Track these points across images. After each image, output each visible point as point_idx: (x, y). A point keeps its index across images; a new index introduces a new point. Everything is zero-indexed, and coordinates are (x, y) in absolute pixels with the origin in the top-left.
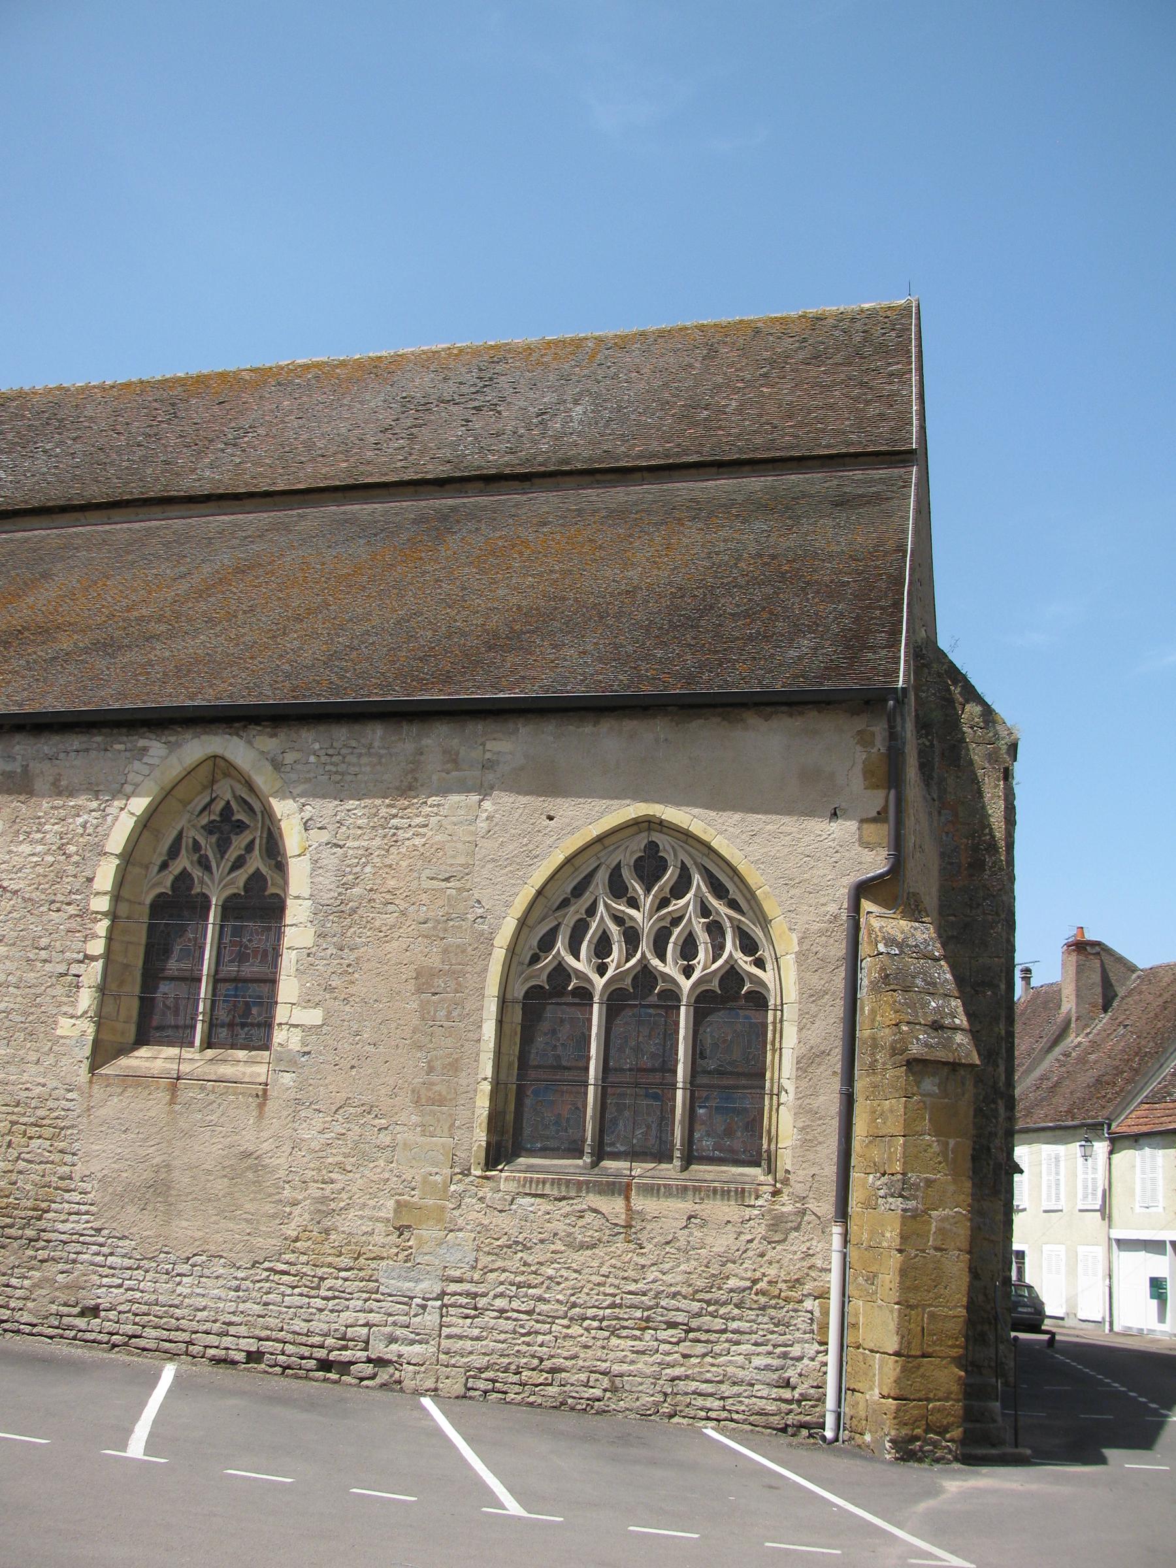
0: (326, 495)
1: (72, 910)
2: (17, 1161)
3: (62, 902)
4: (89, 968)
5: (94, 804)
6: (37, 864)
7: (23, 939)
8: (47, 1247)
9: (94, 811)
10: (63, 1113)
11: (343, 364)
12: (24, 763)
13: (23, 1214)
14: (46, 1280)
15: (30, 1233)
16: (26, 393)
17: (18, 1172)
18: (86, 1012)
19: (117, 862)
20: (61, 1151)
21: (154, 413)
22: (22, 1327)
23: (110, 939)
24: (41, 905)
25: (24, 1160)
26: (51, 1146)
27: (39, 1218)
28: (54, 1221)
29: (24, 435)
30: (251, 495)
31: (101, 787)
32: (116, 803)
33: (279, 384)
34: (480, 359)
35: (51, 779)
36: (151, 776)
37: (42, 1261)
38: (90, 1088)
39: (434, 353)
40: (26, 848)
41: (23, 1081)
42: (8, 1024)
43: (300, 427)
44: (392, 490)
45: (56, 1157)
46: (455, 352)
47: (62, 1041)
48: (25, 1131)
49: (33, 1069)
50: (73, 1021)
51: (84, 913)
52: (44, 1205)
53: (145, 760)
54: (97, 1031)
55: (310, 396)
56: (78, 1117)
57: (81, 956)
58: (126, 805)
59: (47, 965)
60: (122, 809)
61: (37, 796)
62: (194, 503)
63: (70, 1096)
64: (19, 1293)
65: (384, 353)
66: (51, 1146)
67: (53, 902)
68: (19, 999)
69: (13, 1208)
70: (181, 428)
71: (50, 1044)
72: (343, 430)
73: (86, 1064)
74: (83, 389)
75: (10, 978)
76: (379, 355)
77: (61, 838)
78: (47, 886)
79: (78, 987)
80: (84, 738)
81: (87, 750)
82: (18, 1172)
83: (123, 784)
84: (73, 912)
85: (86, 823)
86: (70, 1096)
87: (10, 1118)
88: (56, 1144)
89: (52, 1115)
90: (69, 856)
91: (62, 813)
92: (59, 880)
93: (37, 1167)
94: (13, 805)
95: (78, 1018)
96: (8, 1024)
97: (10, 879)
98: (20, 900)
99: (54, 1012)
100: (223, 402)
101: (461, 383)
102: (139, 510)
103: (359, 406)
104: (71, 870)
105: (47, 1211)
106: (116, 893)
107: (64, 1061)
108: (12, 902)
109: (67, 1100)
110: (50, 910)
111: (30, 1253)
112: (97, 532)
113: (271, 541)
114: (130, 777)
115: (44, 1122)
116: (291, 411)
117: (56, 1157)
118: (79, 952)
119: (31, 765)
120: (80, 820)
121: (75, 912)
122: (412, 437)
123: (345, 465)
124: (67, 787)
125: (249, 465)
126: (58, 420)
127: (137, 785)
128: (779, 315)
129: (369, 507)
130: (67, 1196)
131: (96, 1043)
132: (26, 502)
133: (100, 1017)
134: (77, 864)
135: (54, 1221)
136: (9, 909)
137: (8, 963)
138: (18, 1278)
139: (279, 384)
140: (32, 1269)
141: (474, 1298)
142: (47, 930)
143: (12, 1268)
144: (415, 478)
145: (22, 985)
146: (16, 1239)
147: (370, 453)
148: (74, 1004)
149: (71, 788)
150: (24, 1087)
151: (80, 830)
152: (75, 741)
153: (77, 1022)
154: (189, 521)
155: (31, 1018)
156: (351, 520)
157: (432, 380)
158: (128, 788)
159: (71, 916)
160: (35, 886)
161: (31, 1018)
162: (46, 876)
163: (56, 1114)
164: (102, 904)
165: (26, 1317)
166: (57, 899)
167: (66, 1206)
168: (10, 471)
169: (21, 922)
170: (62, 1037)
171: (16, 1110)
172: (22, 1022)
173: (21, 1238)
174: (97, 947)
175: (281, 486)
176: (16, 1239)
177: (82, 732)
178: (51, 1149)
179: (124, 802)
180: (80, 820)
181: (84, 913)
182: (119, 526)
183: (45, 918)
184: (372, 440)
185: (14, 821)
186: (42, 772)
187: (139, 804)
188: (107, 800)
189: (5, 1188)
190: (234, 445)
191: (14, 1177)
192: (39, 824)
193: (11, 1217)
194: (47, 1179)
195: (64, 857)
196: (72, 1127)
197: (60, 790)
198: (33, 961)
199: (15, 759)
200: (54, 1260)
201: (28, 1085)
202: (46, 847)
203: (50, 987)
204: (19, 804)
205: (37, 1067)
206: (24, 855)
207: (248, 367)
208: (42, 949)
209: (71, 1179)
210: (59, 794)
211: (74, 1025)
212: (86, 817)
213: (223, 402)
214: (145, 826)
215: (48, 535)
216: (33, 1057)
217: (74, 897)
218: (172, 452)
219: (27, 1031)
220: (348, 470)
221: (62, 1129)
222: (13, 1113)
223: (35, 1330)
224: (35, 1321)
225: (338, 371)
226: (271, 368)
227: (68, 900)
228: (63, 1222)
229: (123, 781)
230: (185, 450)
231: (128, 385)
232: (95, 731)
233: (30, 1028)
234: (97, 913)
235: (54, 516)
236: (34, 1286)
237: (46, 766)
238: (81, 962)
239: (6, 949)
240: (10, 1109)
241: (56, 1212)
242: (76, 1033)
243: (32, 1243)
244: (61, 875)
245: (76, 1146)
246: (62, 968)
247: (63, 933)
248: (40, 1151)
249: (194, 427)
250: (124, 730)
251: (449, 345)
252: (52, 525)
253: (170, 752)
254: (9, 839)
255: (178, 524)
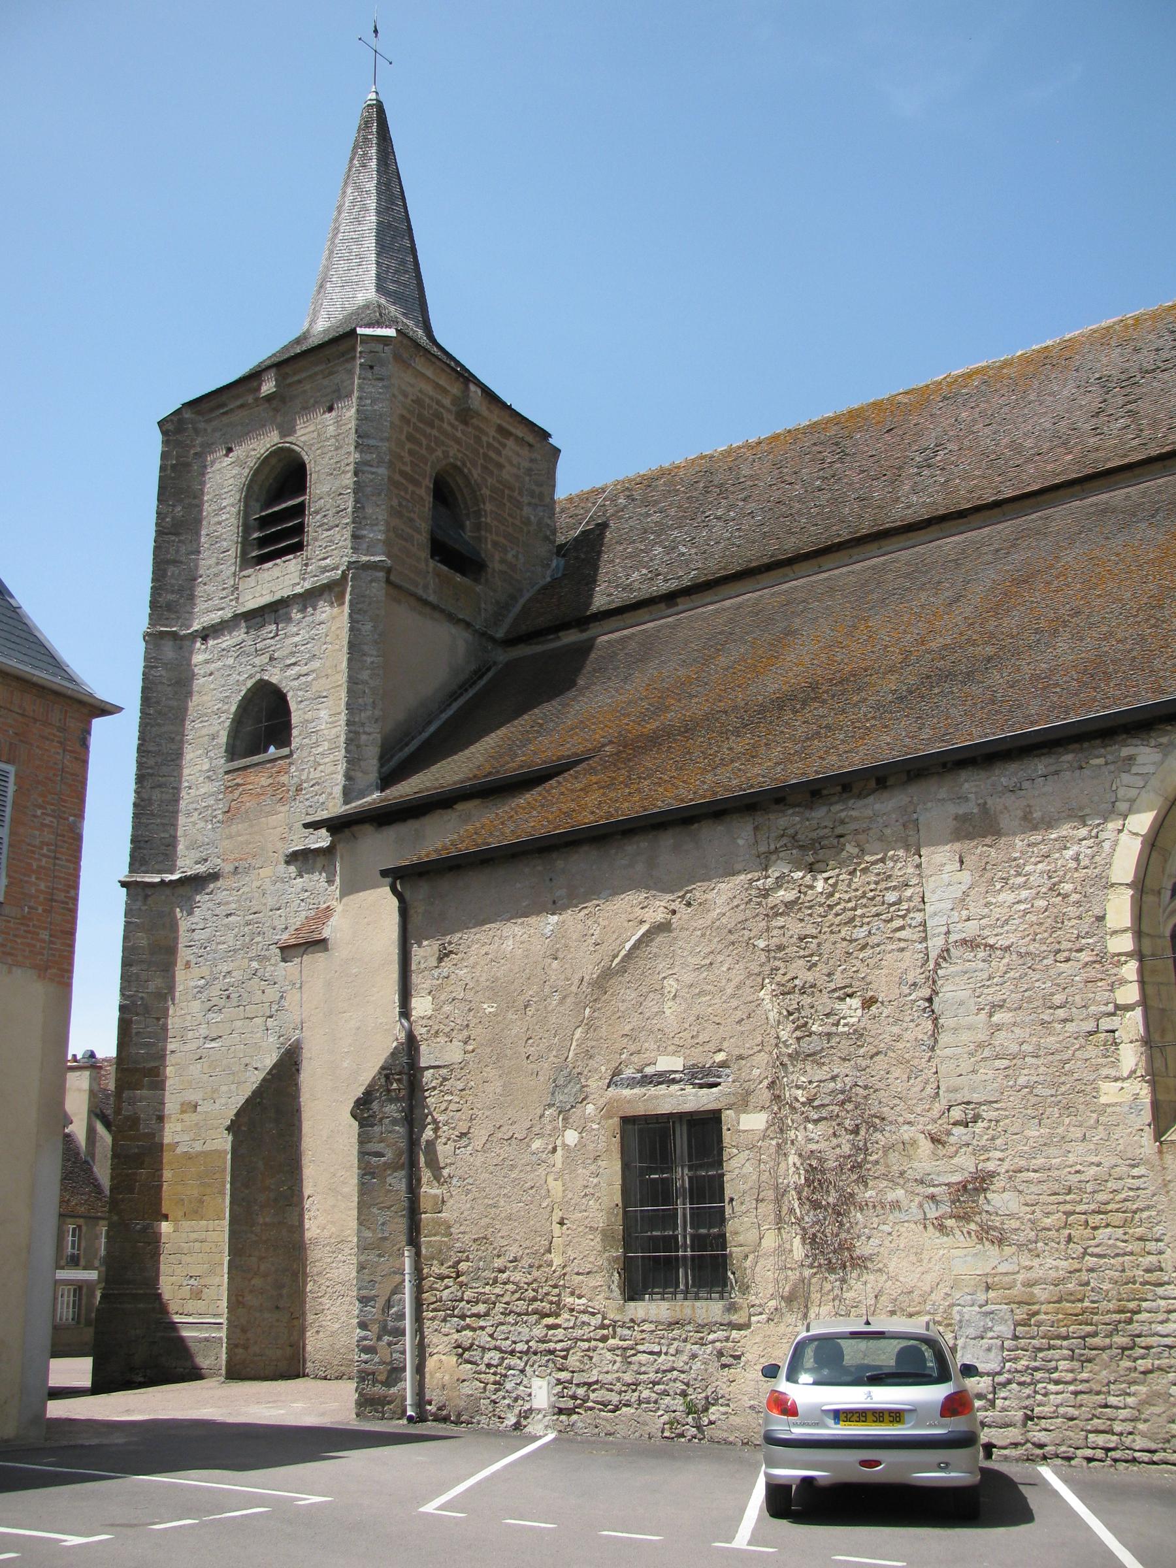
0: (1061, 493)
1: (1085, 956)
2: (1083, 1258)
3: (1070, 950)
4: (1125, 1020)
5: (1083, 832)
6: (1026, 913)
7: (1030, 1000)
8: (1148, 1354)
9: (1085, 839)
10: (1131, 1193)
11: (1007, 364)
12: (980, 801)
13: (1107, 1318)
14: (1158, 1395)
15: (1120, 1340)
16: (669, 470)
17: (1088, 1270)
18: (1134, 1072)
19: (1130, 892)
20: (1140, 1239)
21: (820, 456)
22: (1137, 1454)
23: (1142, 982)
24: (1044, 958)
25: (1092, 1255)
26: (1125, 1234)
27: (1130, 1321)
28: (1150, 1323)
29: (688, 508)
30: (977, 509)
31: (1087, 811)
32: (1111, 826)
33: (945, 398)
34: (1165, 322)
35: (1020, 813)
36: (1148, 787)
37: (1144, 1373)
38: (1161, 1159)
39: (1108, 328)
40: (1007, 897)
41: (1071, 1163)
42: (1033, 1100)
43: (994, 433)
44: (1137, 471)
45: (1135, 1246)
46: (1130, 322)
47: (1109, 1110)
48: (1087, 1222)
49: (1080, 1148)
50: (1119, 1084)
51: (1102, 957)
52: (1132, 1305)
53: (1134, 770)
54: (1154, 1092)
55: (987, 402)
56: (1154, 1195)
57: (1111, 1007)
58: (1124, 825)
59: (1068, 1025)
60: (1120, 831)
61: (1007, 835)
62: (913, 531)
63: (1135, 1172)
64: (1123, 1414)
65: (1049, 343)
66: (1125, 1234)
67: (1059, 951)
68: (1042, 1069)
69: (1092, 1313)
70: (858, 464)
71: (1094, 1115)
72: (1048, 425)
73: (1148, 1133)
74: (729, 452)
75: (1024, 1047)
76: (1044, 345)
77: (1050, 877)
78: (1046, 935)
79: (1116, 1044)
80: (1046, 760)
81: (1057, 773)
82: (1088, 1270)
83: (1114, 803)
84: (1088, 959)
85: (1078, 854)
86: (1135, 1172)
87: (1062, 1208)
88: (1131, 1231)
89: (1119, 1197)
90: (1066, 896)
91: (1044, 849)
92: (1060, 925)
93: (1112, 1261)
94: (978, 851)
95: (1124, 1079)
96: (1033, 1100)
97: (996, 935)
98: (1014, 957)
99: (1092, 1078)
100: (891, 429)
101: (1157, 350)
102: (851, 551)
103: (1052, 398)
104: (1072, 911)
105: (1138, 1312)
106: (1136, 929)
107: (1118, 1132)
108: (1005, 961)
109: (1133, 1177)
110: (1056, 961)
111: (1126, 1363)
112: (815, 582)
113: (1029, 547)
114: (1121, 792)
115: (1109, 1207)
116: (974, 421)
117: (1135, 1246)
118: (1106, 1004)
119: (990, 802)
120: (1069, 853)
121: (1091, 959)
122: (1132, 414)
123: (1070, 457)
124: (1043, 818)
125: (957, 481)
126: (716, 486)
127: (1132, 801)
128: (984, 364)
129: (1120, 493)
130: (1160, 1291)
131: (1156, 1105)
132: (724, 569)
133: (1153, 1075)
134: (1078, 903)
135: (1150, 1323)
136: (1003, 969)
137: (1017, 1030)
138: (1117, 1396)
139: (945, 398)
140: (1134, 1383)
141: (1134, 1362)
142: (1058, 985)
143: (1108, 1385)
144: (1163, 451)
145: (1041, 1053)
146: (1103, 1349)
147: (1092, 440)
148: (1115, 1064)
149: (1048, 819)
150: (1073, 1170)
151: (1073, 864)
152: (1040, 766)
153: (1125, 1085)
154: (916, 549)
155: (1063, 1089)
156: (1105, 511)
157: (1122, 355)
158: (1122, 806)
159: (1087, 964)
160: (1031, 937)
161: (1063, 1089)
162: (1041, 923)
163: (1123, 1196)
164: (1125, 943)
165: (1140, 1443)
166: (1062, 948)
167: (1162, 1303)
168: (689, 544)
169: (1022, 981)
170: (1108, 1105)
171: (1068, 1198)
172: (1052, 1096)
173: (1110, 1347)
174: (1130, 993)
175: (1009, 493)
176: (1103, 1349)
177: (1043, 754)
178: (1126, 1237)
179: (1121, 822)
180: (1069, 853)
181: (1102, 957)
182: (836, 572)
183: (1052, 972)
184: (1088, 427)
185: (985, 869)
186: (1006, 808)
187: (1142, 821)
188: (1099, 825)
189: (1075, 1291)
190: (929, 466)
191: (1084, 1276)
192: (1018, 866)
193: (1091, 1324)
194: (1129, 1274)
195: (1060, 898)
196: (1148, 1208)
197: (1030, 823)
198: (1049, 1023)
199: (967, 799)
200: (1162, 1370)
201: (1079, 1167)
202: (1034, 891)
203: (1078, 1049)
204: (985, 848)
205: (1083, 1144)
206: (1006, 904)
207: (901, 390)
208: (1058, 1007)
209: (1161, 1270)
210: (1035, 828)
211: (1122, 1088)
212: (1076, 848)
213: (891, 429)
214: (1153, 845)
215: (761, 596)
216: (1077, 1133)
217: (1083, 941)
218: (861, 489)
219: (1061, 1105)
220: (1075, 462)
221: (1135, 1212)
222: (1065, 1202)
223: (1156, 1458)
224: (1153, 1446)
225: (1005, 371)
226: (927, 386)
227: (1078, 946)
228: (1161, 1322)
229: (1113, 800)
230: (875, 483)
231: (776, 437)
232: (1061, 750)
233: (1064, 1101)
234: (1119, 954)
235: (759, 577)
236: (1143, 1403)
237: (1009, 799)
238: (1113, 1014)
239: (1011, 1014)
240: (1060, 1198)
241: (1149, 1312)
242: (1126, 1097)
243: (1126, 1353)
244: (1060, 920)
245: (1158, 1230)
246: (1090, 1026)
247: (1081, 985)
248: (1111, 1242)
249: (871, 459)
250: (1098, 742)
251: (1120, 318)
252: (759, 586)
253: (1165, 755)
254: (983, 890)
255: (905, 555)
